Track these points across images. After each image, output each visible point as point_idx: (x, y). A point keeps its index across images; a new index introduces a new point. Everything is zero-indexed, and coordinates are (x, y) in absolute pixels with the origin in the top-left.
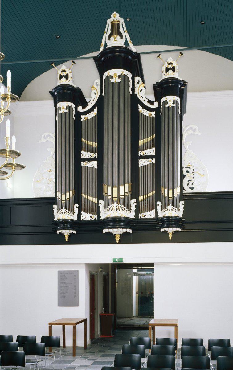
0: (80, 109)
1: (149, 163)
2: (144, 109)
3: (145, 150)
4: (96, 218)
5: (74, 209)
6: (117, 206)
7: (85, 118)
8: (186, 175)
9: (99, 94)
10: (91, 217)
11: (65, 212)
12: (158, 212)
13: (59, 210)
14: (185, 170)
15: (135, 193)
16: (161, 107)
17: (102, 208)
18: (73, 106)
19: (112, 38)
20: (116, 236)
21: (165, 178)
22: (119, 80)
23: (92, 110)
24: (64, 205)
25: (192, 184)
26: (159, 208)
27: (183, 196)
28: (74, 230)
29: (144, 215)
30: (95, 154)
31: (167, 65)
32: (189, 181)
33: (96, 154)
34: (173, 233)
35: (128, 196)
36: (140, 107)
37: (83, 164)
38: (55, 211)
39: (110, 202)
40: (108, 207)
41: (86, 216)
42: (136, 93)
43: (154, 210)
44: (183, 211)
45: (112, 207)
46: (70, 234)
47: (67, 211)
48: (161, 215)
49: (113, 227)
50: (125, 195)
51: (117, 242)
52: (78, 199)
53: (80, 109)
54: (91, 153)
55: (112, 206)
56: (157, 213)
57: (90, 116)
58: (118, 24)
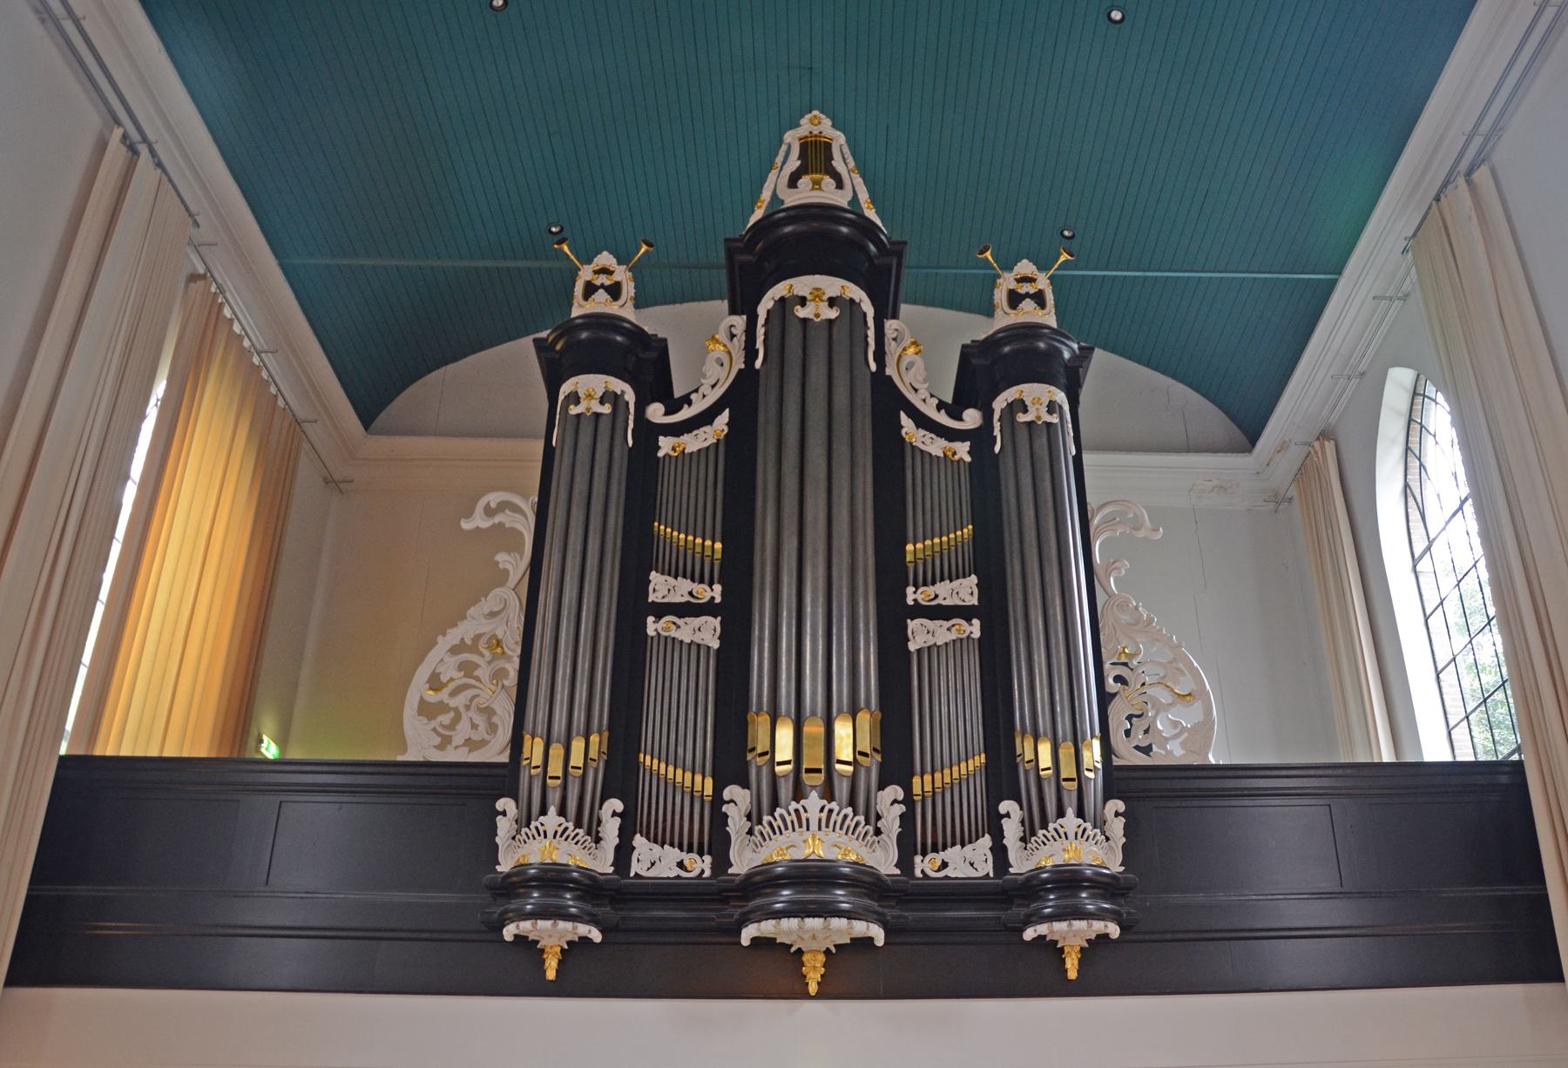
0: (656, 412)
1: (953, 636)
2: (922, 432)
3: (933, 583)
4: (703, 871)
5: (599, 822)
6: (822, 810)
7: (674, 449)
8: (1114, 695)
9: (739, 364)
10: (681, 865)
11: (560, 830)
12: (1005, 849)
13: (525, 820)
14: (1110, 673)
15: (895, 756)
16: (997, 425)
17: (736, 823)
18: (630, 397)
19: (805, 181)
20: (805, 958)
21: (1031, 690)
22: (833, 314)
23: (706, 418)
24: (554, 798)
25: (1146, 731)
26: (1012, 830)
27: (1117, 780)
28: (593, 920)
29: (939, 863)
30: (711, 586)
31: (1013, 285)
32: (1129, 718)
33: (718, 588)
34: (1082, 950)
35: (868, 770)
36: (905, 420)
37: (652, 626)
38: (504, 826)
39: (785, 790)
40: (776, 814)
41: (656, 861)
42: (888, 371)
43: (986, 841)
44: (1124, 847)
45: (797, 811)
46: (569, 943)
47: (571, 825)
48: (1020, 864)
49: (799, 910)
50: (855, 763)
51: (813, 988)
52: (621, 773)
53: (656, 412)
54: (693, 580)
55: (799, 806)
56: (1000, 853)
57: (694, 442)
58: (828, 146)
